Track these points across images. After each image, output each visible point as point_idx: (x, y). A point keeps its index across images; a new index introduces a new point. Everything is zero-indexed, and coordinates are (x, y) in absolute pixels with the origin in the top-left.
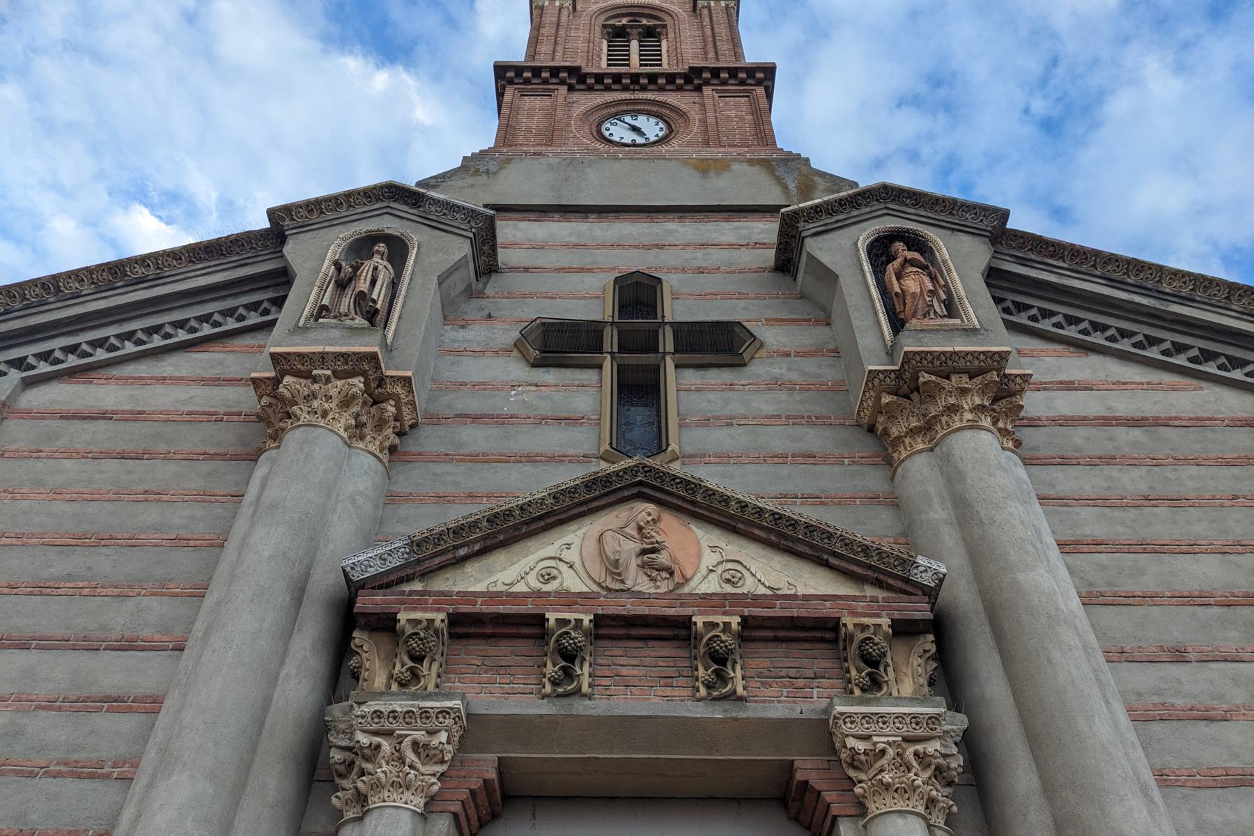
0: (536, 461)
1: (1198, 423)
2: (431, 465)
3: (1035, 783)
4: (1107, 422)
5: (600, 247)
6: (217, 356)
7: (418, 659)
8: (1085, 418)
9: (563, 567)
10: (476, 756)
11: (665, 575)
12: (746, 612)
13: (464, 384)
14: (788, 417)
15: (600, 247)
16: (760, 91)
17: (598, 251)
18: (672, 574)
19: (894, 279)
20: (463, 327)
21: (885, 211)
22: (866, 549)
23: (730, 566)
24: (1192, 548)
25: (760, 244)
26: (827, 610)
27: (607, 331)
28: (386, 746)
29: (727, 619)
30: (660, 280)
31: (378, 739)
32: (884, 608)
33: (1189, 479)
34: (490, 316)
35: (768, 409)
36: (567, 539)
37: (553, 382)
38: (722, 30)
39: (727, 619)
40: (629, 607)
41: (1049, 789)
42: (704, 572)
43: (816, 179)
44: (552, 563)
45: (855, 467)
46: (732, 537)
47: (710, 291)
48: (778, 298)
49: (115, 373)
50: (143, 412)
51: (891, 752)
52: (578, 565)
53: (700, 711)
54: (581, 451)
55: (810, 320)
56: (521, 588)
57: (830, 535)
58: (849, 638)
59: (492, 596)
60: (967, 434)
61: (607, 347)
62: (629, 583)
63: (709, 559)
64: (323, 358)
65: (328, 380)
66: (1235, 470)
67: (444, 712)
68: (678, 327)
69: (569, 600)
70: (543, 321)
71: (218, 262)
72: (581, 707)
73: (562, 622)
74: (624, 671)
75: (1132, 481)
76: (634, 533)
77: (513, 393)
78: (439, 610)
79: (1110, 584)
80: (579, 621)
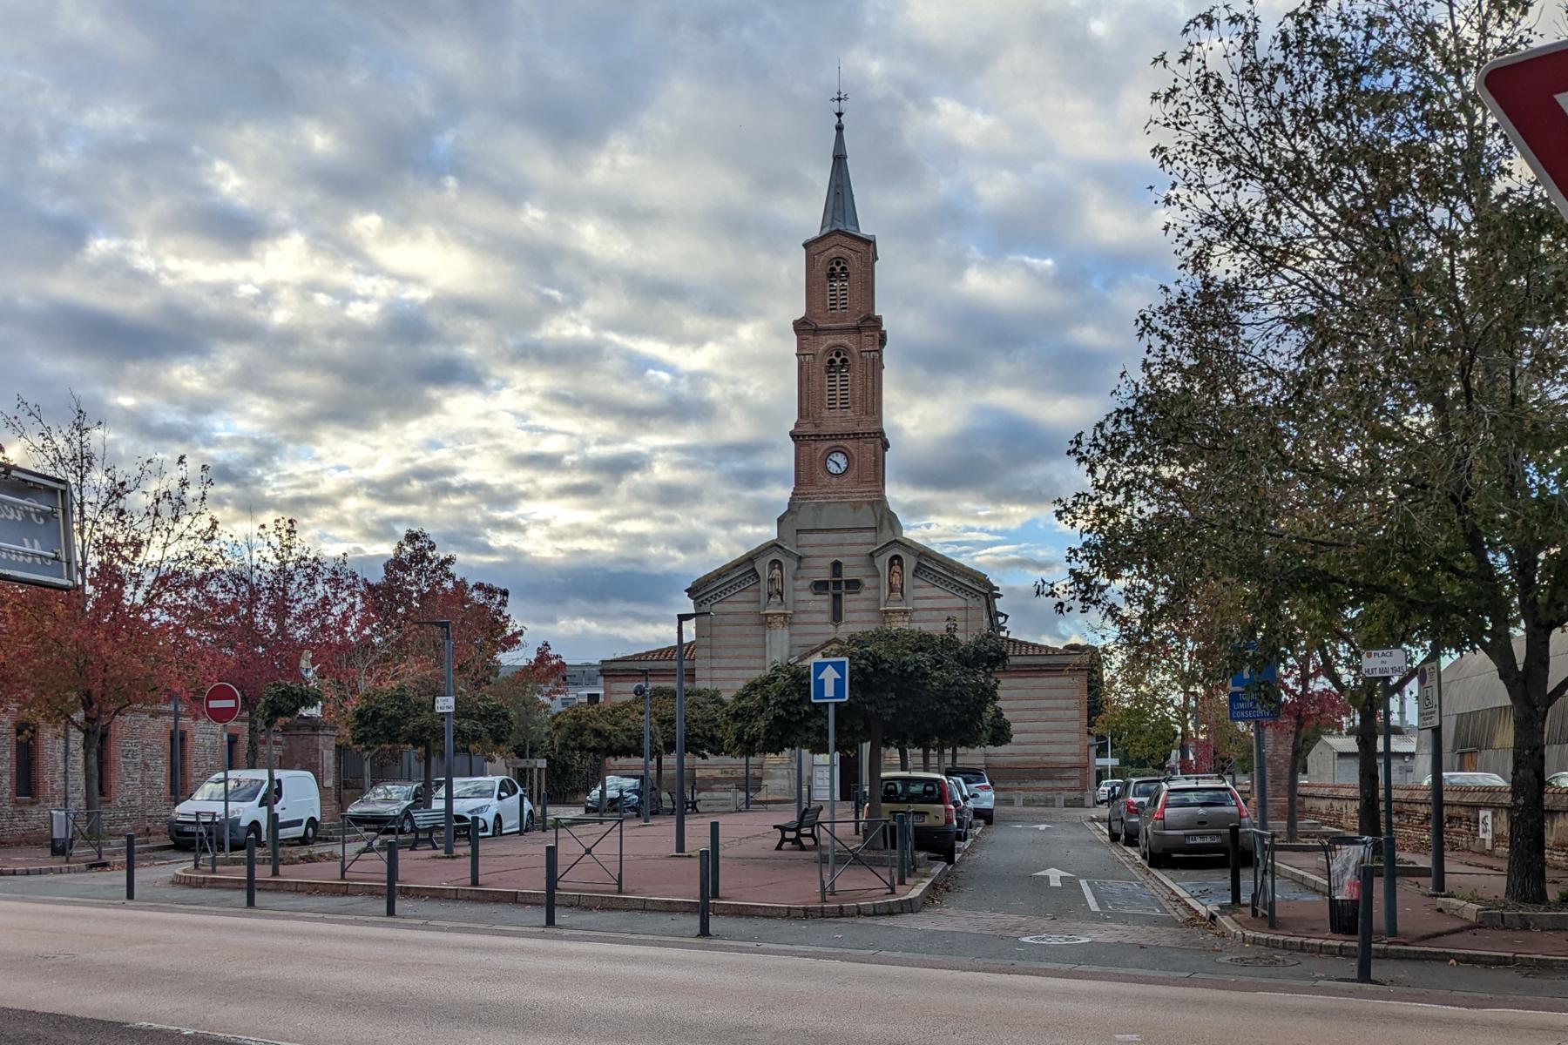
4: (932, 609)
68: (847, 581)
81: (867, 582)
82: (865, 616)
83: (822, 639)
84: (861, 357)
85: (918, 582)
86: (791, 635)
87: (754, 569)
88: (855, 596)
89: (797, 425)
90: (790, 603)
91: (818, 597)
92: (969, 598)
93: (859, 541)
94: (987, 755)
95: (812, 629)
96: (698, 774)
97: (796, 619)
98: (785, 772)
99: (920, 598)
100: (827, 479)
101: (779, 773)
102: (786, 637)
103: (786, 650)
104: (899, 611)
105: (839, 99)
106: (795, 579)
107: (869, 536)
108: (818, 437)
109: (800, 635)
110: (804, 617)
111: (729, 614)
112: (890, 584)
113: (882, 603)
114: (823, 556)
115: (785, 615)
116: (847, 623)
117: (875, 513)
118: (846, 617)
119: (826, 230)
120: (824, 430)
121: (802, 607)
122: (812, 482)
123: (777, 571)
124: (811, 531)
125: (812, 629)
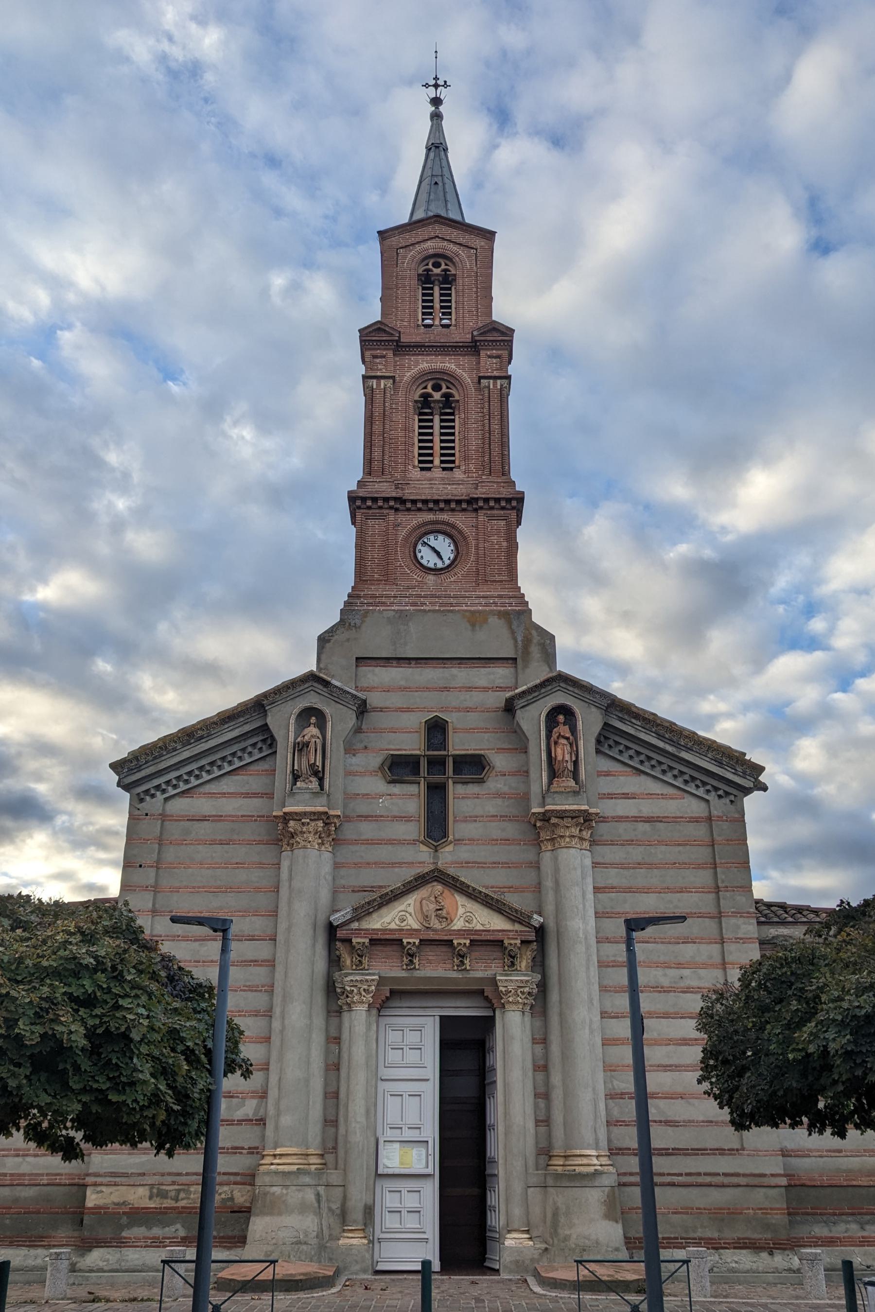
0: (393, 844)
1: (675, 820)
2: (350, 847)
3: (558, 999)
4: (636, 819)
5: (418, 689)
6: (245, 778)
7: (361, 956)
8: (628, 817)
9: (408, 915)
10: (382, 988)
11: (444, 920)
12: (472, 937)
13: (358, 795)
14: (501, 816)
15: (418, 689)
16: (514, 514)
17: (416, 694)
18: (447, 919)
19: (553, 745)
20: (354, 755)
21: (558, 688)
22: (516, 911)
23: (468, 914)
24: (647, 890)
25: (499, 687)
26: (500, 936)
27: (422, 759)
28: (355, 991)
29: (465, 941)
30: (447, 722)
31: (352, 988)
32: (519, 935)
33: (662, 853)
34: (366, 747)
35: (493, 811)
36: (408, 902)
37: (398, 793)
38: (495, 404)
39: (465, 941)
40: (432, 936)
41: (560, 1002)
42: (459, 917)
43: (534, 633)
44: (403, 913)
45: (525, 847)
46: (470, 900)
47: (472, 727)
48: (503, 732)
49: (201, 790)
50: (221, 816)
51: (513, 991)
52: (413, 914)
53: (454, 975)
54: (412, 838)
55: (517, 749)
56: (393, 926)
57: (505, 904)
58: (506, 948)
59: (384, 931)
60: (565, 850)
61: (422, 774)
62: (432, 924)
63: (461, 911)
64: (305, 814)
65: (308, 824)
66: (681, 848)
67: (373, 980)
68: (455, 757)
69: (412, 932)
70: (392, 752)
71: (234, 723)
72: (417, 974)
73: (409, 943)
74: (430, 958)
75: (636, 853)
76: (433, 899)
77: (381, 800)
78: (366, 937)
79: (612, 908)
80: (414, 943)
81: (499, 761)
82: (496, 830)
83: (408, 874)
84: (479, 389)
85: (605, 764)
86: (337, 866)
87: (265, 728)
88: (473, 789)
89: (360, 484)
90: (338, 797)
91: (396, 789)
92: (712, 797)
93: (483, 683)
94: (785, 1153)
95: (383, 853)
96: (92, 1199)
97: (349, 831)
98: (310, 1195)
99: (611, 796)
100: (416, 576)
101: (294, 1196)
102: (327, 869)
103: (325, 895)
104: (574, 815)
105: (436, 86)
106: (350, 750)
107: (501, 674)
108: (401, 504)
109: (357, 865)
110: (367, 830)
111: (204, 819)
112: (550, 759)
113: (535, 798)
114: (409, 710)
115: (325, 817)
116: (458, 841)
117: (513, 633)
118: (456, 830)
119: (420, 215)
120: (409, 493)
121: (362, 808)
122: (387, 577)
123: (313, 731)
124: (387, 661)
125: (383, 853)
